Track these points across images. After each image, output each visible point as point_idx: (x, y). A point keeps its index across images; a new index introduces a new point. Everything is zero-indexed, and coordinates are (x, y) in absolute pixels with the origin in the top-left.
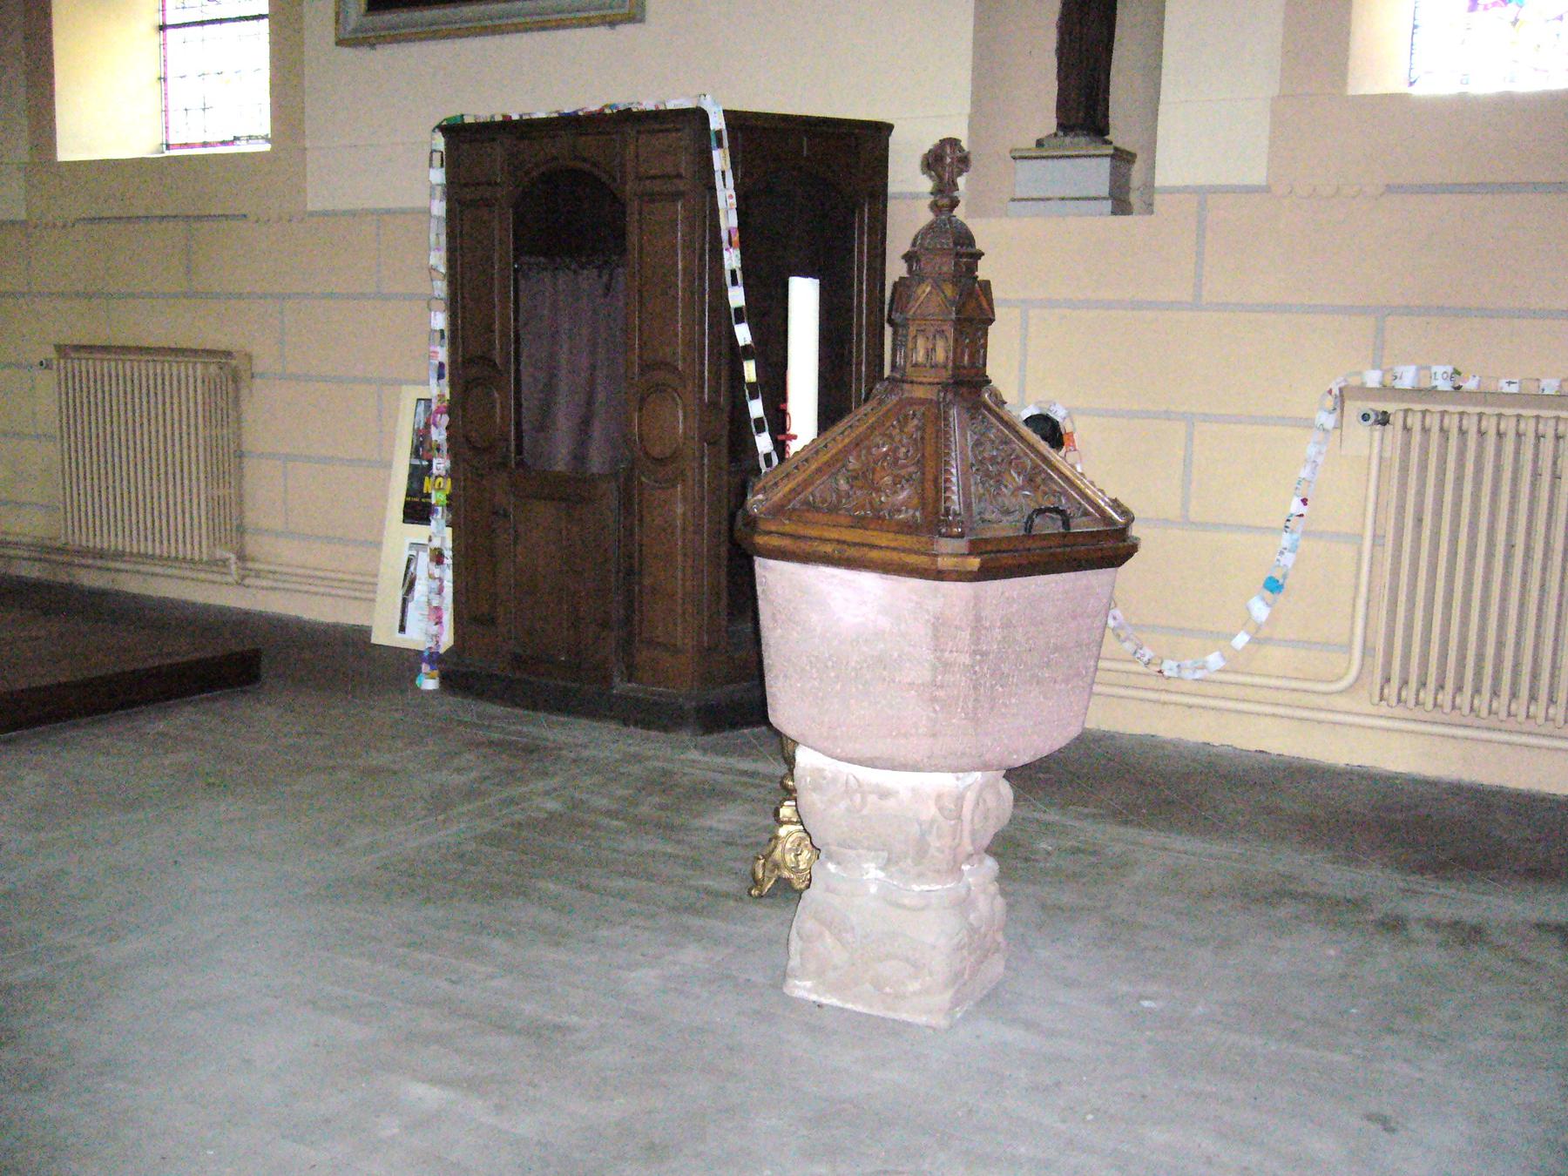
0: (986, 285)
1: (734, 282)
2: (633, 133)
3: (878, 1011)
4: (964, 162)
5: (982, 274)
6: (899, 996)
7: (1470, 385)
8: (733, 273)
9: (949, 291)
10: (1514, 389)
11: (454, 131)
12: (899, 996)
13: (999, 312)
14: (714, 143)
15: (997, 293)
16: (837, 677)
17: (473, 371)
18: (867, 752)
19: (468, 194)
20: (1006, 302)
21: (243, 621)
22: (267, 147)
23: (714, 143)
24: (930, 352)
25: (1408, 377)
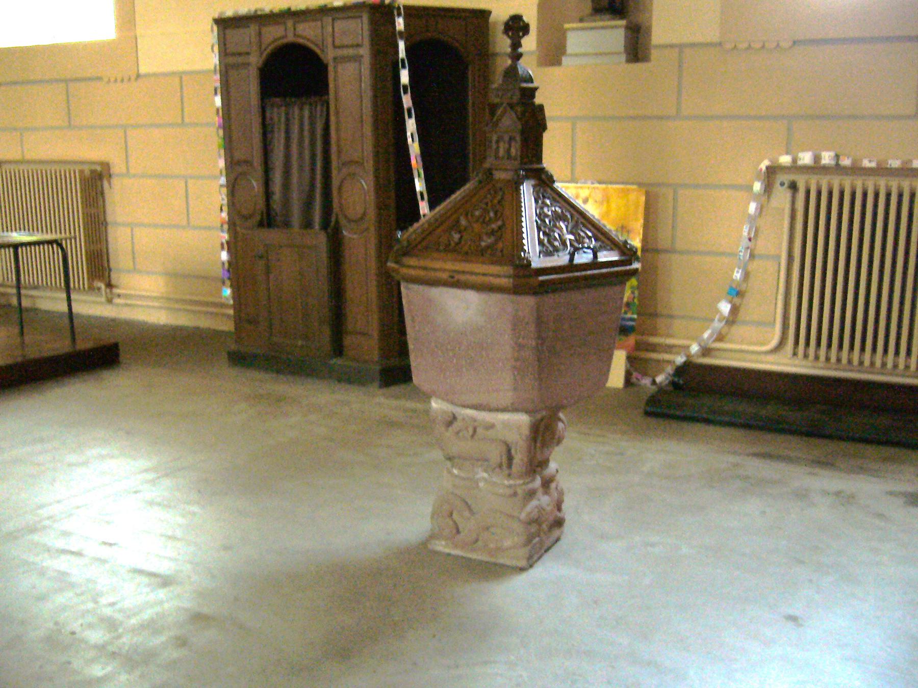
0: (541, 108)
1: (422, 198)
2: (330, 20)
3: (485, 558)
4: (525, 29)
5: (538, 100)
6: (499, 550)
7: (846, 162)
8: (422, 194)
9: (519, 109)
10: (873, 165)
11: (224, 24)
12: (499, 550)
13: (549, 124)
14: (396, 13)
15: (548, 113)
16: (454, 356)
17: (240, 169)
18: (475, 401)
19: (230, 60)
20: (552, 118)
21: (113, 323)
22: (567, 26)
23: (396, 13)
24: (508, 151)
25: (806, 158)
